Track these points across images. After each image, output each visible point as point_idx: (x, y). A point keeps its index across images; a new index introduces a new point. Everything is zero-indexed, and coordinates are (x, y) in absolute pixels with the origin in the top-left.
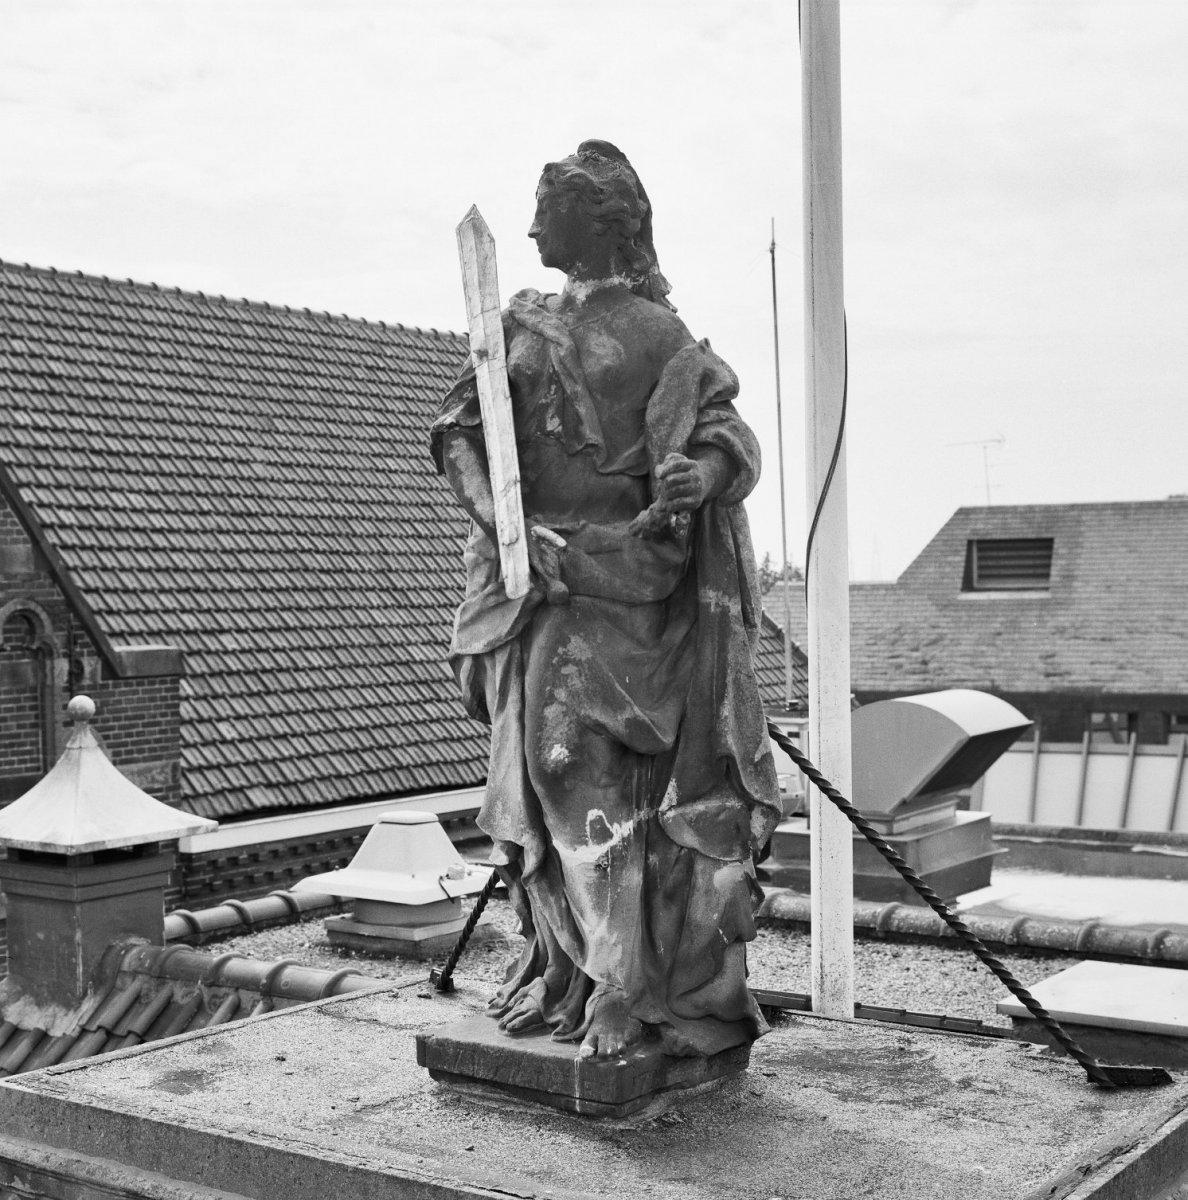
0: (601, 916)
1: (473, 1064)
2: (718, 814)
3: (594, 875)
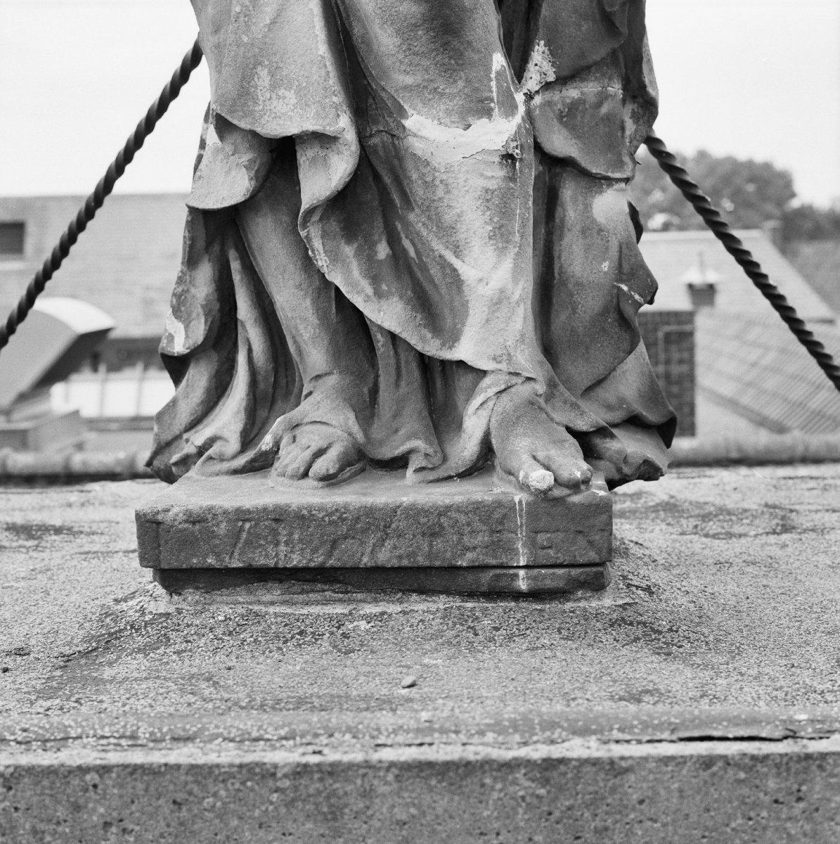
0: (501, 251)
1: (277, 544)
2: (599, 105)
3: (501, 173)
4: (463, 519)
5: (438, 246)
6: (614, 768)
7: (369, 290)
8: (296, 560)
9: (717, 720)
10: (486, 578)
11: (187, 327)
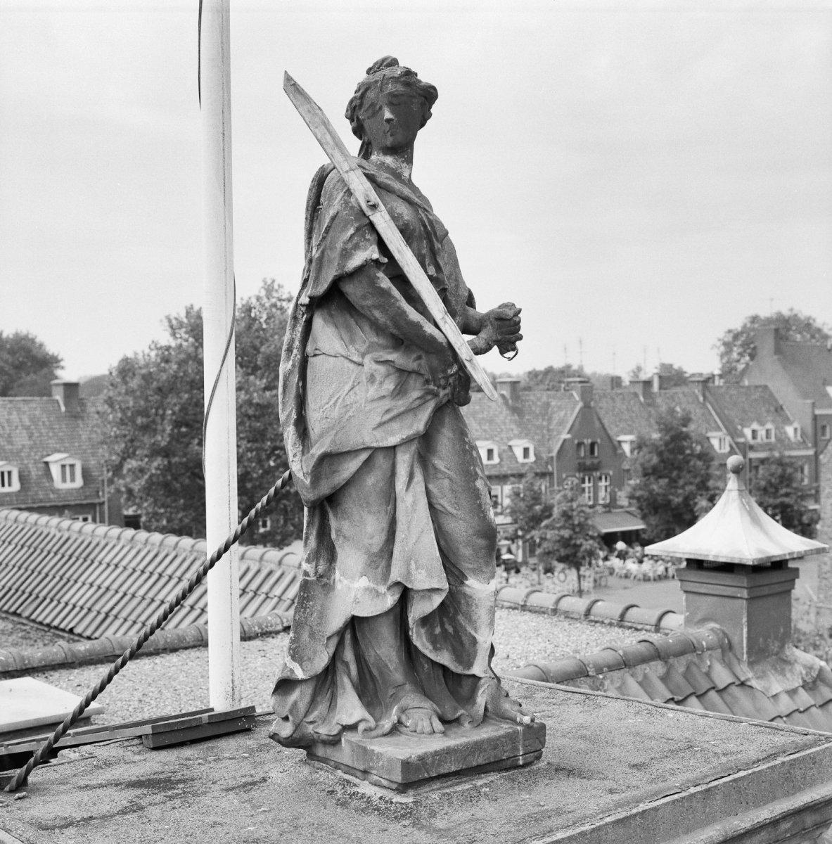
4: (504, 740)
5: (470, 629)
6: (656, 809)
7: (431, 647)
8: (453, 769)
9: (669, 789)
10: (509, 762)
11: (301, 665)
